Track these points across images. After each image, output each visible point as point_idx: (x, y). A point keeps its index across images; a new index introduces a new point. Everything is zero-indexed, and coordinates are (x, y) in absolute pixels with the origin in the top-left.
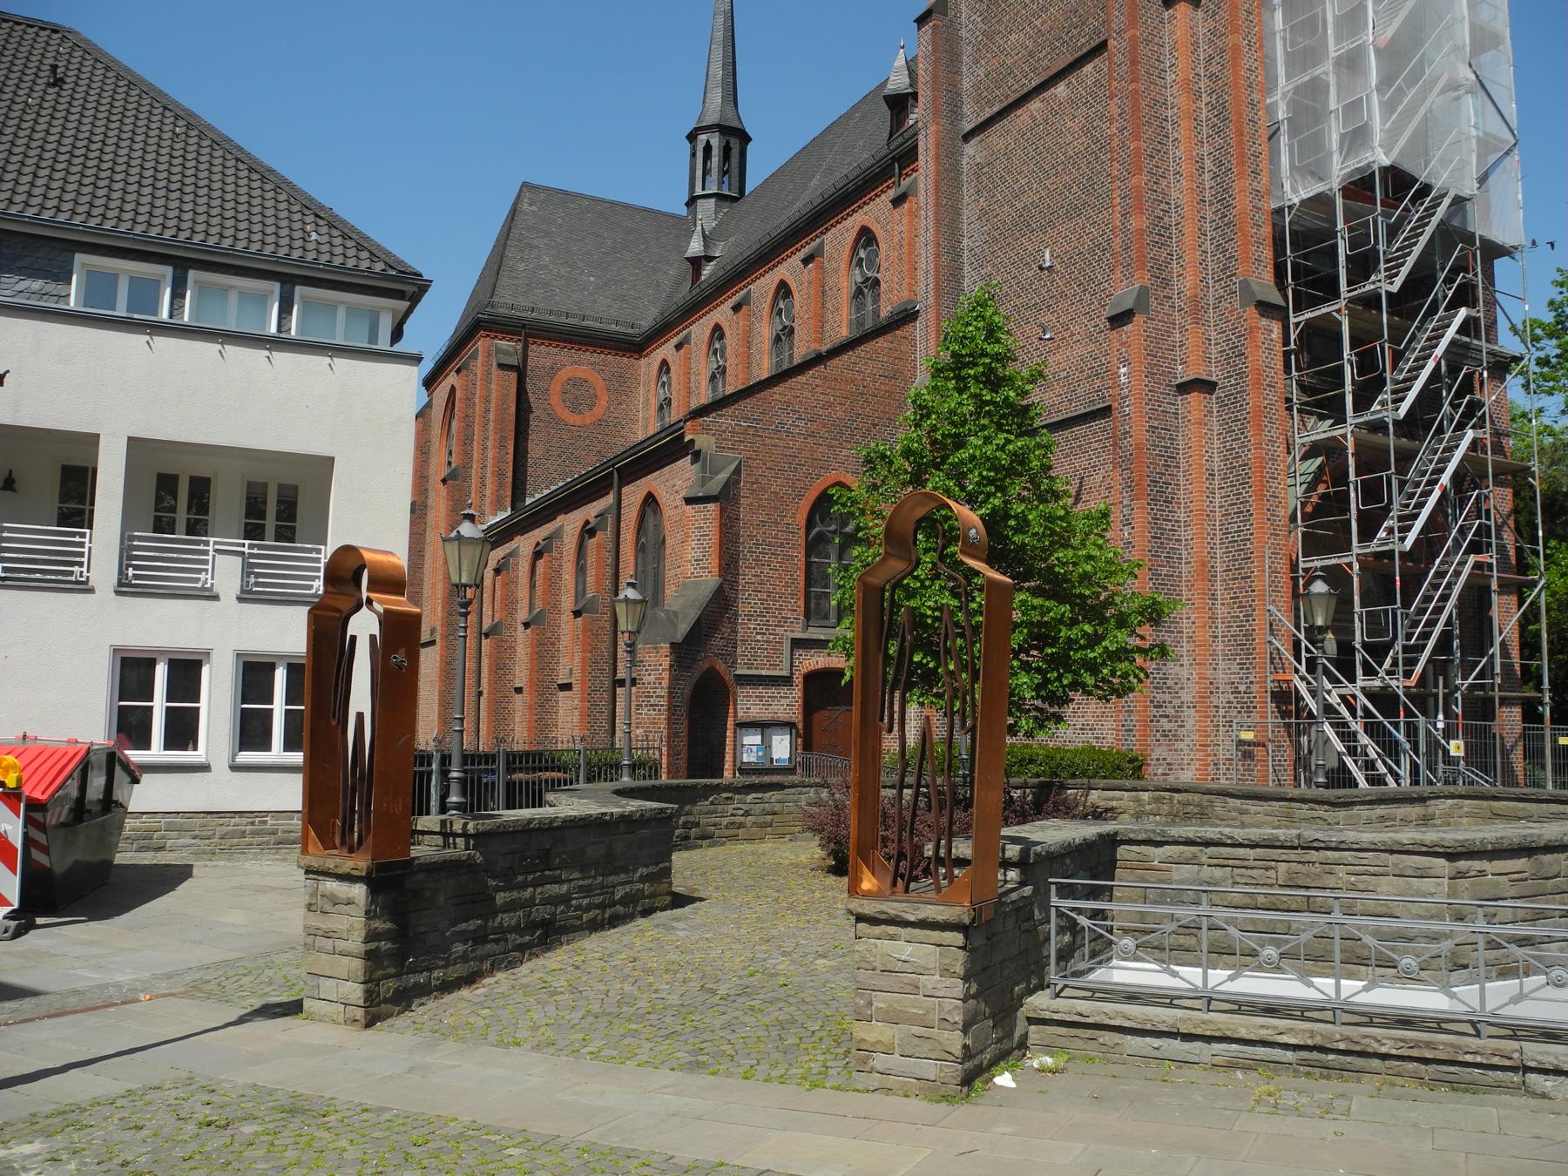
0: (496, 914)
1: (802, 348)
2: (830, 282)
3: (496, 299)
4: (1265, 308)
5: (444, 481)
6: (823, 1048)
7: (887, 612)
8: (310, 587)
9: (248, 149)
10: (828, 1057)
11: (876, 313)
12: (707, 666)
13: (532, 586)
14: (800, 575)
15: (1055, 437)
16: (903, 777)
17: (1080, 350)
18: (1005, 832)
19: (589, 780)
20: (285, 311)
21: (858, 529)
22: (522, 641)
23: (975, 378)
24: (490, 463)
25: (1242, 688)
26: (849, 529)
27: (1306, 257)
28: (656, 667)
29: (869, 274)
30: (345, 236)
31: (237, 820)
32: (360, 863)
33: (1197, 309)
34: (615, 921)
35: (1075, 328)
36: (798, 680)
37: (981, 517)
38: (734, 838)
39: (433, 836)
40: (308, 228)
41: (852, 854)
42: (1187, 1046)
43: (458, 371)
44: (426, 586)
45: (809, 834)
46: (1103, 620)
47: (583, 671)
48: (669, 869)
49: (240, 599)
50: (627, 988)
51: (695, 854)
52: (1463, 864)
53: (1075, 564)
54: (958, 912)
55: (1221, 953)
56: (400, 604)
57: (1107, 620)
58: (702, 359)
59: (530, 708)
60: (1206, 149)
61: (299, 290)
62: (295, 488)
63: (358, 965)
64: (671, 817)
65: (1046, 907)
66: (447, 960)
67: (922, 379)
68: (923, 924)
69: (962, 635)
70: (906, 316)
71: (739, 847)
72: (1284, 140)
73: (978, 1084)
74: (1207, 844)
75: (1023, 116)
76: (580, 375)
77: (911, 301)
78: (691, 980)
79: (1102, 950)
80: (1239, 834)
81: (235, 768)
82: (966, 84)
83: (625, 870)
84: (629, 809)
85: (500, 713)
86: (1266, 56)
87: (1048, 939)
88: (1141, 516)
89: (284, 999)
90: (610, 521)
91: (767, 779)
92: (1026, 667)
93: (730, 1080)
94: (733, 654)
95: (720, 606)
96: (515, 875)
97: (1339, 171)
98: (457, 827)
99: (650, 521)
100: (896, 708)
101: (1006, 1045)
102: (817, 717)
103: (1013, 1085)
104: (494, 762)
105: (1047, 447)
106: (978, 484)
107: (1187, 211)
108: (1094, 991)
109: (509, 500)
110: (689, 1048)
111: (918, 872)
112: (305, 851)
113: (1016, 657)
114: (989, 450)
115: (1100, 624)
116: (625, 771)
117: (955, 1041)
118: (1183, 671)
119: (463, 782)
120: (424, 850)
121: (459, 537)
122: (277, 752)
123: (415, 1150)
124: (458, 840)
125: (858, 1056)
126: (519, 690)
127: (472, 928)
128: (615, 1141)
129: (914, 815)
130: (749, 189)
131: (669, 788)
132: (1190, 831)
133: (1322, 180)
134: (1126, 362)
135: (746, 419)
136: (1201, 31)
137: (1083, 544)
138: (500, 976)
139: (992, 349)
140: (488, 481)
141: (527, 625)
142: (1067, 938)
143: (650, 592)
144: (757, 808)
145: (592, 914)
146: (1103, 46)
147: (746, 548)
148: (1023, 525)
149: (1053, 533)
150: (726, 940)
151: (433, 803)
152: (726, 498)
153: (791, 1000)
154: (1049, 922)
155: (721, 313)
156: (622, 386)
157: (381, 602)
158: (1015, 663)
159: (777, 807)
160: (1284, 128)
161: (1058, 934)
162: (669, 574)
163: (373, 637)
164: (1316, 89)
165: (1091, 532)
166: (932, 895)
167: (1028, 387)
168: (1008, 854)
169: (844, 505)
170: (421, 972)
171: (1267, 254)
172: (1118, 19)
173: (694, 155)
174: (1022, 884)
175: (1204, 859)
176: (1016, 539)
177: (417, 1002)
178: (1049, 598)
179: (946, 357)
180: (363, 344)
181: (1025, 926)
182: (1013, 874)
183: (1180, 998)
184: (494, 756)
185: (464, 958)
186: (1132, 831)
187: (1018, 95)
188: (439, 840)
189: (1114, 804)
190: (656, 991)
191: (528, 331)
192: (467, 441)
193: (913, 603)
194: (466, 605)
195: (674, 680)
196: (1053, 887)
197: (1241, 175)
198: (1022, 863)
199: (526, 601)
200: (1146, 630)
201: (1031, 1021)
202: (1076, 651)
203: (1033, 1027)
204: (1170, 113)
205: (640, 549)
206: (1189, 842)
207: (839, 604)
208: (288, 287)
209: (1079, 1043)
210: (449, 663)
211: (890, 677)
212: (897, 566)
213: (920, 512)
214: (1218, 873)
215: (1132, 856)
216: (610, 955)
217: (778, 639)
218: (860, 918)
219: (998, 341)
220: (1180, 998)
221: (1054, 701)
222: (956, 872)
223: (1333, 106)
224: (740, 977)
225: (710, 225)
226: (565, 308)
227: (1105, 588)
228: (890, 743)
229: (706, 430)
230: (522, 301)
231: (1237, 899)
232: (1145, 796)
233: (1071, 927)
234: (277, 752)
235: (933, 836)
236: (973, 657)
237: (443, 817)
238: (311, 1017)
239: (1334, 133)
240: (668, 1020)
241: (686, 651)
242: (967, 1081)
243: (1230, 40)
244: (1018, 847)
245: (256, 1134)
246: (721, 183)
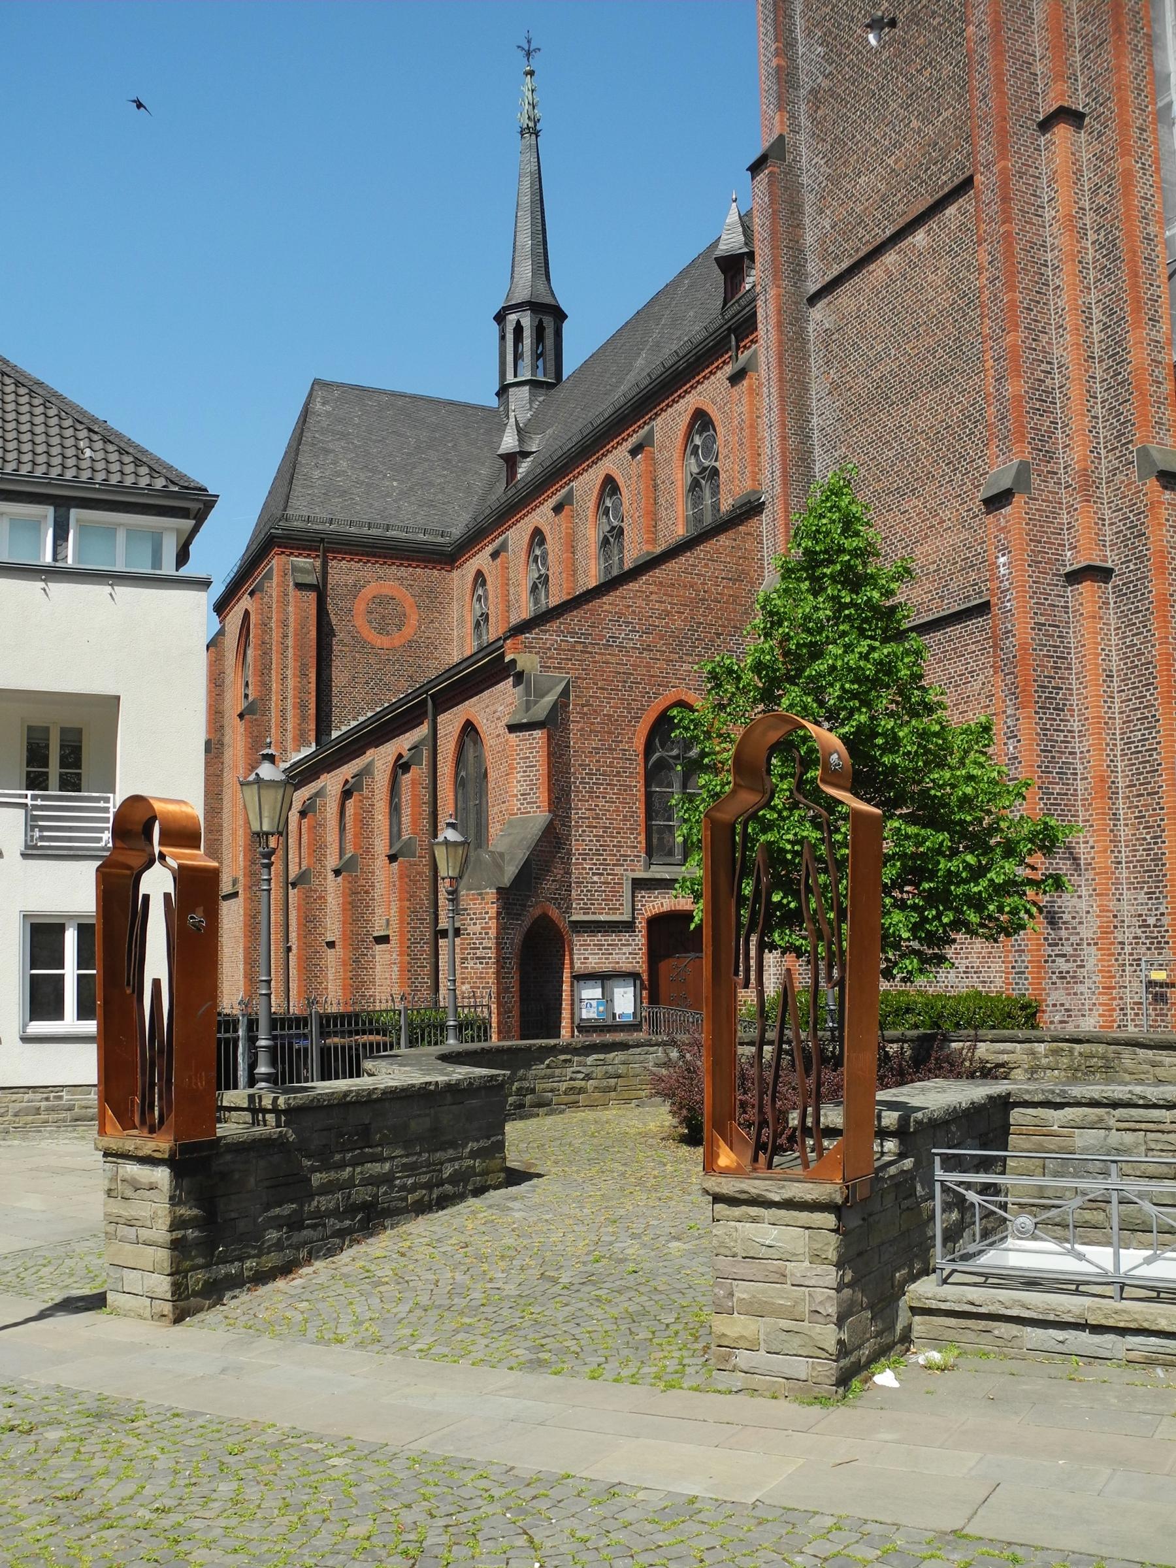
0: (311, 1196)
1: (633, 551)
2: (662, 475)
3: (290, 512)
5: (241, 716)
6: (677, 1342)
7: (739, 848)
8: (99, 840)
9: (13, 361)
10: (685, 1353)
11: (716, 507)
12: (537, 912)
13: (342, 829)
14: (640, 807)
15: (926, 639)
16: (763, 1031)
17: (951, 539)
18: (881, 1096)
19: (412, 1043)
20: (60, 536)
21: (703, 754)
22: (333, 890)
23: (832, 577)
24: (290, 694)
25: (1151, 921)
26: (694, 752)
28: (481, 916)
29: (706, 463)
30: (121, 451)
31: (30, 1096)
32: (162, 1144)
33: (1087, 485)
34: (443, 1202)
35: (945, 514)
36: (641, 924)
37: (844, 738)
38: (574, 1104)
39: (242, 1112)
40: (81, 444)
41: (706, 1120)
42: (1097, 1339)
43: (252, 594)
44: (226, 833)
45: (659, 1099)
46: (988, 850)
47: (401, 921)
48: (502, 1143)
49: (25, 856)
50: (459, 1277)
51: (532, 1123)
53: (953, 786)
54: (830, 1190)
55: (1135, 1229)
56: (198, 858)
57: (992, 849)
58: (522, 568)
60: (1093, 296)
61: (74, 513)
62: (79, 732)
63: (163, 1255)
64: (501, 1085)
65: (930, 1182)
66: (260, 1248)
67: (771, 581)
68: (789, 1204)
69: (825, 871)
70: (751, 509)
71: (581, 1115)
73: (855, 1383)
74: (1115, 1105)
75: (877, 271)
76: (385, 591)
77: (755, 492)
78: (529, 1267)
79: (994, 1229)
80: (1153, 1093)
81: (26, 1039)
82: (809, 238)
83: (453, 1144)
84: (456, 1077)
85: (311, 970)
86: (1163, 181)
87: (932, 1218)
88: (1028, 727)
89: (87, 1291)
91: (609, 1037)
92: (902, 905)
93: (575, 1381)
94: (568, 899)
95: (552, 844)
96: (332, 1153)
98: (267, 1103)
99: (470, 753)
100: (753, 953)
101: (886, 1339)
102: (663, 966)
103: (896, 1384)
104: (306, 1025)
105: (918, 653)
106: (840, 698)
107: (1072, 370)
108: (986, 1276)
109: (313, 734)
110: (529, 1344)
111: (783, 1140)
112: (102, 1131)
113: (888, 894)
114: (852, 659)
115: (984, 854)
116: (451, 1033)
117: (829, 1336)
118: (1080, 903)
119: (272, 1050)
120: (231, 1129)
121: (259, 781)
122: (70, 1022)
123: (231, 1460)
124: (268, 1116)
125: (719, 1354)
126: (331, 945)
127: (286, 1213)
128: (449, 1450)
129: (777, 1076)
130: (566, 372)
131: (500, 1051)
132: (1094, 1091)
134: (1005, 550)
135: (573, 634)
136: (1085, 156)
137: (962, 763)
138: (318, 1264)
139: (851, 543)
140: (290, 714)
141: (337, 872)
142: (955, 1216)
143: (472, 832)
144: (599, 1071)
145: (417, 1195)
146: (968, 183)
147: (578, 776)
148: (893, 744)
149: (927, 751)
150: (568, 1222)
151: (240, 1073)
152: (553, 723)
153: (642, 1289)
154: (933, 1198)
155: (541, 516)
156: (433, 601)
157: (175, 857)
158: (888, 901)
159: (622, 1070)
161: (944, 1211)
162: (493, 811)
163: (167, 896)
165: (971, 748)
166: (799, 1170)
167: (894, 586)
168: (885, 1122)
169: (687, 729)
170: (232, 1262)
172: (986, 150)
173: (503, 338)
174: (902, 1156)
175: (1112, 1122)
176: (885, 759)
177: (228, 1294)
178: (924, 827)
179: (797, 554)
180: (147, 570)
181: (906, 1204)
182: (891, 1145)
183: (1087, 1283)
184: (305, 1019)
185: (279, 1246)
186: (1027, 1091)
187: (870, 247)
188: (247, 1116)
189: (1006, 1057)
190: (491, 1280)
191: (327, 545)
192: (264, 670)
193: (770, 837)
194: (268, 855)
195: (502, 929)
196: (937, 1159)
197: (1137, 324)
198: (901, 1132)
199: (336, 846)
200: (1038, 859)
201: (914, 1311)
202: (958, 885)
203: (917, 1318)
204: (1049, 256)
205: (460, 783)
206: (1094, 1104)
207: (685, 841)
208: (62, 510)
209: (971, 1336)
210: (254, 917)
211: (744, 920)
212: (749, 798)
213: (774, 736)
214: (1129, 1138)
215: (1028, 1120)
216: (438, 1241)
217: (618, 881)
218: (718, 1198)
219: (857, 534)
220: (1087, 1283)
221: (932, 949)
222: (826, 1143)
224: (585, 1264)
225: (524, 416)
226: (365, 518)
227: (989, 812)
228: (747, 997)
229: (529, 648)
230: (320, 513)
231: (1152, 1169)
232: (1041, 1048)
233: (957, 1202)
234: (70, 1022)
235: (798, 1101)
236: (838, 895)
237: (251, 1091)
238: (115, 1312)
240: (505, 1312)
241: (513, 898)
242: (843, 1380)
243: (1119, 165)
244: (896, 1115)
245: (62, 1441)
246: (535, 368)
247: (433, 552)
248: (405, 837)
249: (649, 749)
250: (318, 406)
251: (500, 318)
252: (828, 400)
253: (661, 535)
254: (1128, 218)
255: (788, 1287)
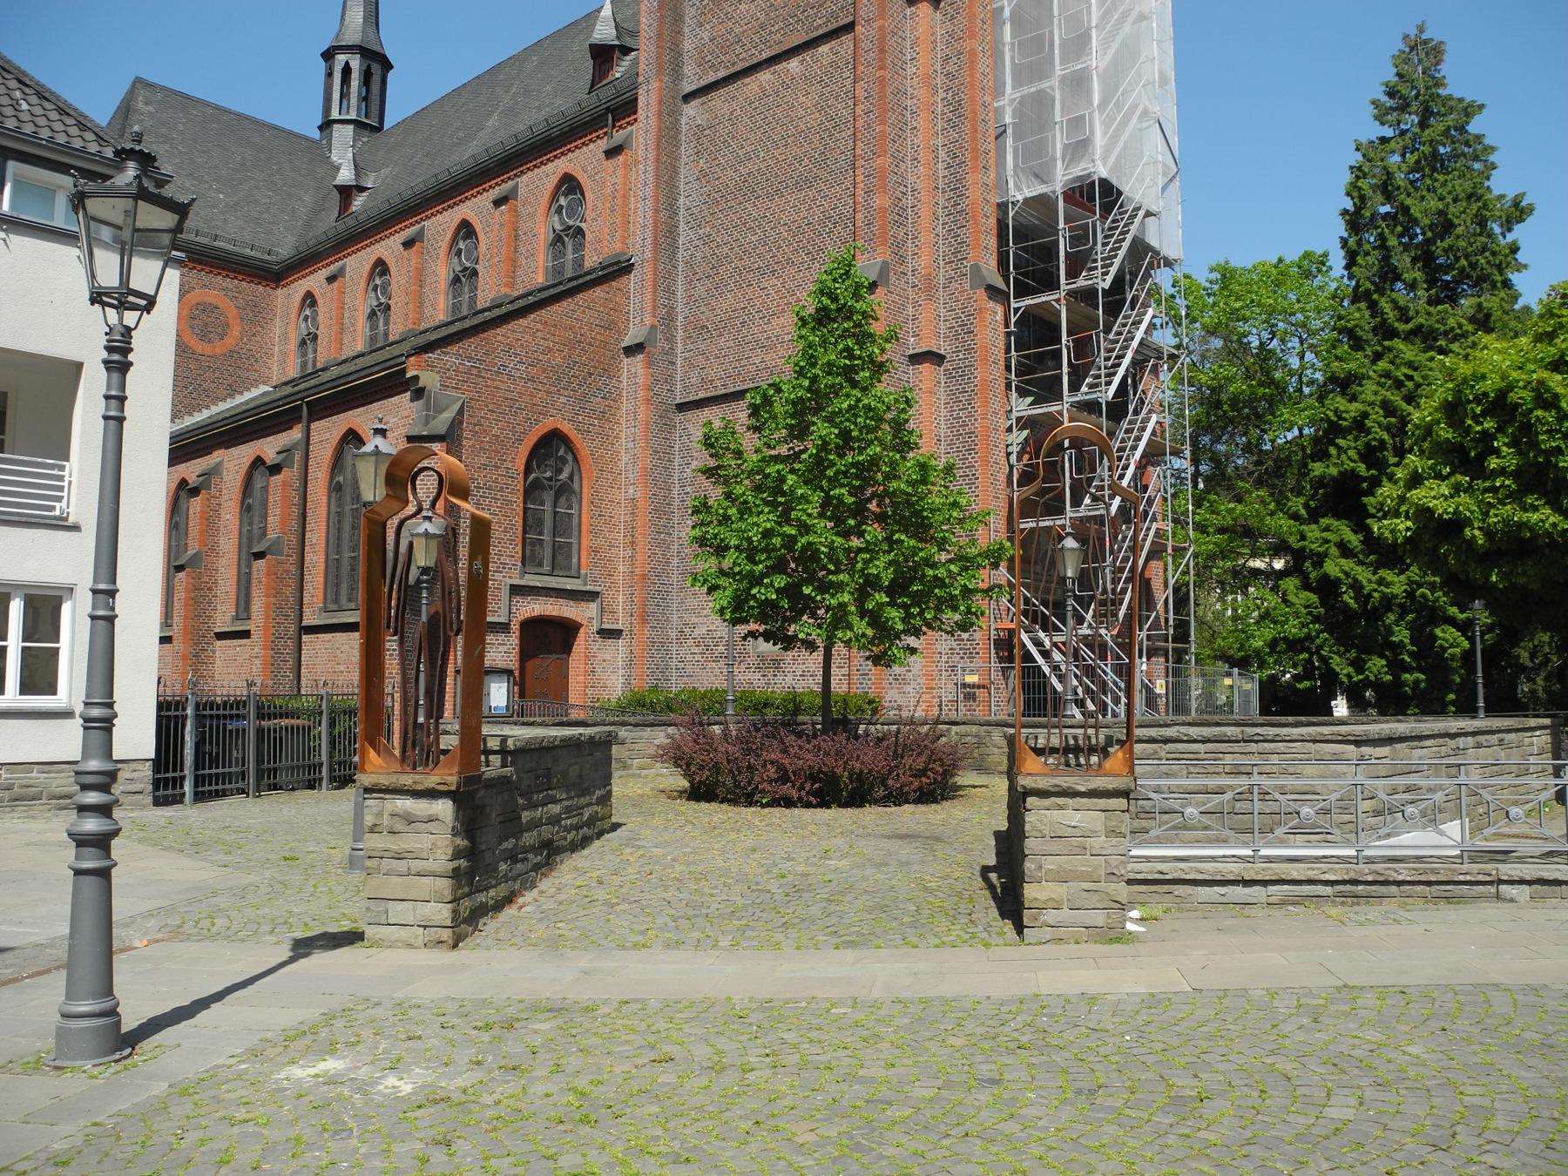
0: (521, 831)
1: (489, 289)
4: (992, 291)
11: (579, 262)
27: (1029, 252)
36: (515, 627)
42: (1248, 890)
47: (267, 616)
52: (1366, 750)
59: (184, 658)
60: (940, 141)
63: (445, 885)
70: (619, 269)
72: (1009, 142)
74: (1166, 741)
75: (752, 84)
82: (688, 45)
90: (297, 457)
97: (1061, 178)
102: (530, 664)
124: (491, 757)
133: (1044, 182)
135: (470, 359)
146: (850, 27)
156: (257, 317)
160: (1010, 131)
164: (1041, 102)
171: (993, 242)
173: (330, 75)
177: (482, 921)
185: (506, 879)
223: (1058, 119)
229: (431, 367)
238: (377, 944)
239: (1059, 143)
247: (260, 269)
248: (272, 535)
249: (528, 470)
250: (140, 105)
251: (328, 55)
252: (696, 185)
253: (519, 280)
254: (972, 86)
255: (1088, 857)
